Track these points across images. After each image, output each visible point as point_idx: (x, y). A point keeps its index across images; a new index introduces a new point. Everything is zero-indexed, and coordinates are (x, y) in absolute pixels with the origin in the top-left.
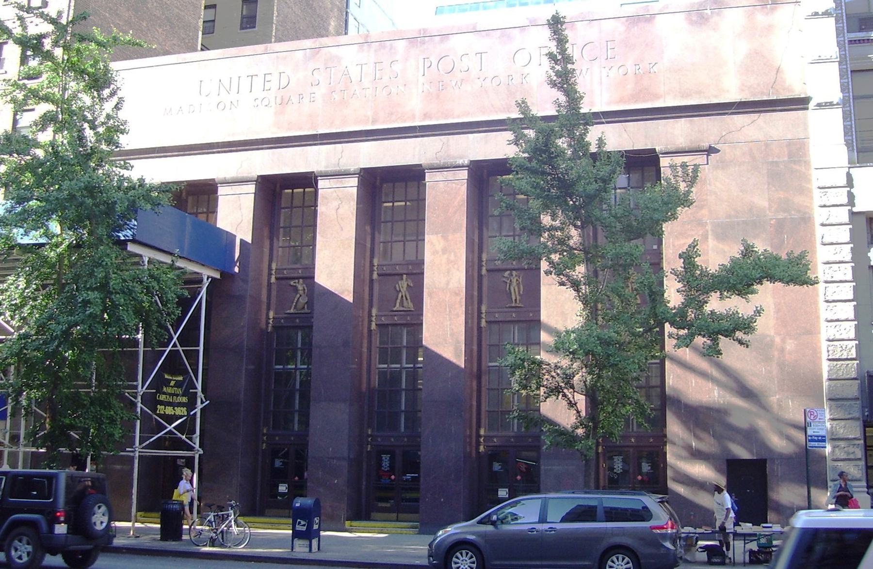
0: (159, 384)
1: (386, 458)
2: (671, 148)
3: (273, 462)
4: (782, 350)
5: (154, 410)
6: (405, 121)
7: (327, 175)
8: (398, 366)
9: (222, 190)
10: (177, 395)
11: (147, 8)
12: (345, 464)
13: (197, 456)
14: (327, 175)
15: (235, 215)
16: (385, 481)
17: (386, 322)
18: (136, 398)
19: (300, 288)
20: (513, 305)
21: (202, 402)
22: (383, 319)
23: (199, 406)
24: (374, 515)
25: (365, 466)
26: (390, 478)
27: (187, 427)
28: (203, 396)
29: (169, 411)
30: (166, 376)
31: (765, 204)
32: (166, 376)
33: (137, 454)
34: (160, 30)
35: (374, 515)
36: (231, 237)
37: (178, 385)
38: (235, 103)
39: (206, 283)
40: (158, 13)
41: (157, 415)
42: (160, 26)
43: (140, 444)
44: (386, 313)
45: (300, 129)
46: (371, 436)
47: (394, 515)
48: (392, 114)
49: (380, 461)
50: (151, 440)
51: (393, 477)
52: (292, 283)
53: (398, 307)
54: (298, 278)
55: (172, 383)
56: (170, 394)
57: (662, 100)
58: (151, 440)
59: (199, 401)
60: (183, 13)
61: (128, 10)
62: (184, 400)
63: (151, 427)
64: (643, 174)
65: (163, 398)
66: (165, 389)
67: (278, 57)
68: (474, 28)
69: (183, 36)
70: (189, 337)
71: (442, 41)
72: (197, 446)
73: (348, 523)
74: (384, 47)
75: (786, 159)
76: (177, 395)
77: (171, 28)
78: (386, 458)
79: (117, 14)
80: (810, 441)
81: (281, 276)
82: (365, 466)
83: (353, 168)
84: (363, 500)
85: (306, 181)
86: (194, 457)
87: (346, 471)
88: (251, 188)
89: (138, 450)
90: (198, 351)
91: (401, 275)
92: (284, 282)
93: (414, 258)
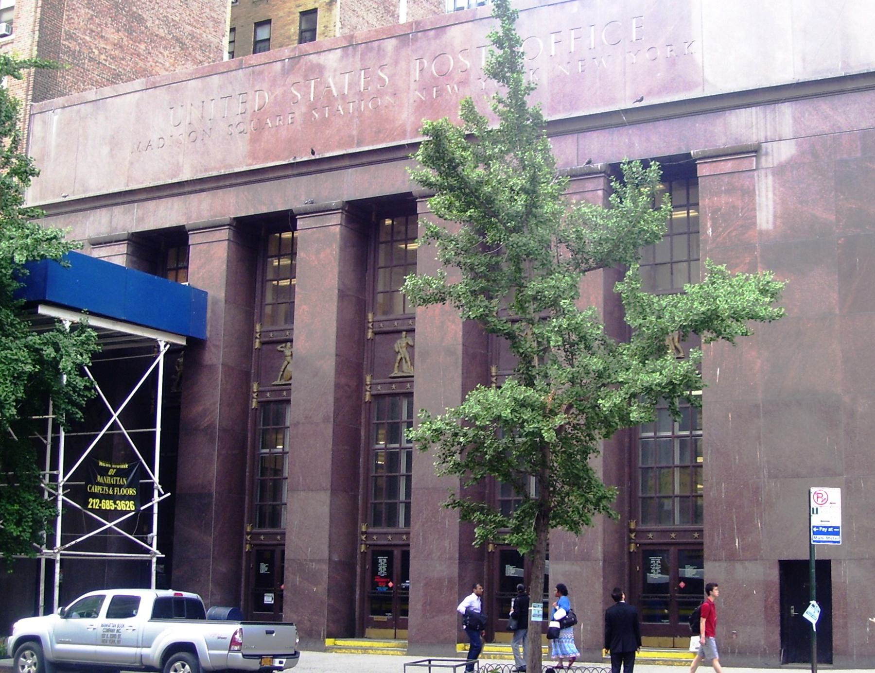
0: (89, 472)
1: (382, 561)
2: (709, 149)
3: (258, 568)
4: (852, 414)
5: (85, 504)
6: (394, 140)
7: (306, 213)
8: (397, 445)
9: (193, 239)
10: (120, 486)
11: (146, 28)
12: (325, 567)
13: (154, 560)
14: (306, 213)
15: (209, 267)
16: (382, 588)
17: (384, 392)
18: (57, 490)
21: (160, 495)
22: (379, 387)
23: (156, 499)
24: (497, 635)
25: (358, 570)
26: (387, 586)
27: (139, 523)
28: (160, 486)
29: (108, 505)
30: (101, 464)
31: (832, 218)
32: (101, 464)
33: (58, 557)
34: (166, 53)
35: (497, 635)
36: (202, 296)
37: (120, 473)
38: (208, 132)
39: (163, 350)
40: (162, 32)
41: (90, 510)
42: (165, 48)
43: (62, 544)
44: (383, 381)
45: (278, 158)
46: (365, 533)
47: (670, 640)
48: (379, 132)
49: (375, 564)
50: (79, 540)
51: (391, 584)
52: (279, 348)
53: (396, 373)
55: (112, 472)
56: (109, 486)
57: (700, 88)
58: (79, 540)
59: (156, 493)
60: (198, 31)
61: (119, 31)
62: (131, 492)
63: (76, 523)
64: (688, 194)
65: (97, 489)
66: (99, 479)
67: (253, 72)
68: (474, 16)
69: (201, 58)
70: (139, 415)
71: (437, 37)
72: (154, 548)
73: (329, 642)
74: (371, 50)
75: (859, 155)
76: (120, 486)
77: (182, 49)
78: (382, 561)
79: (102, 37)
80: (815, 533)
81: (267, 339)
82: (358, 570)
83: (334, 202)
84: (357, 614)
85: (286, 220)
86: (150, 562)
87: (326, 577)
88: (224, 234)
89: (57, 552)
90: (155, 432)
91: (400, 332)
92: (270, 347)
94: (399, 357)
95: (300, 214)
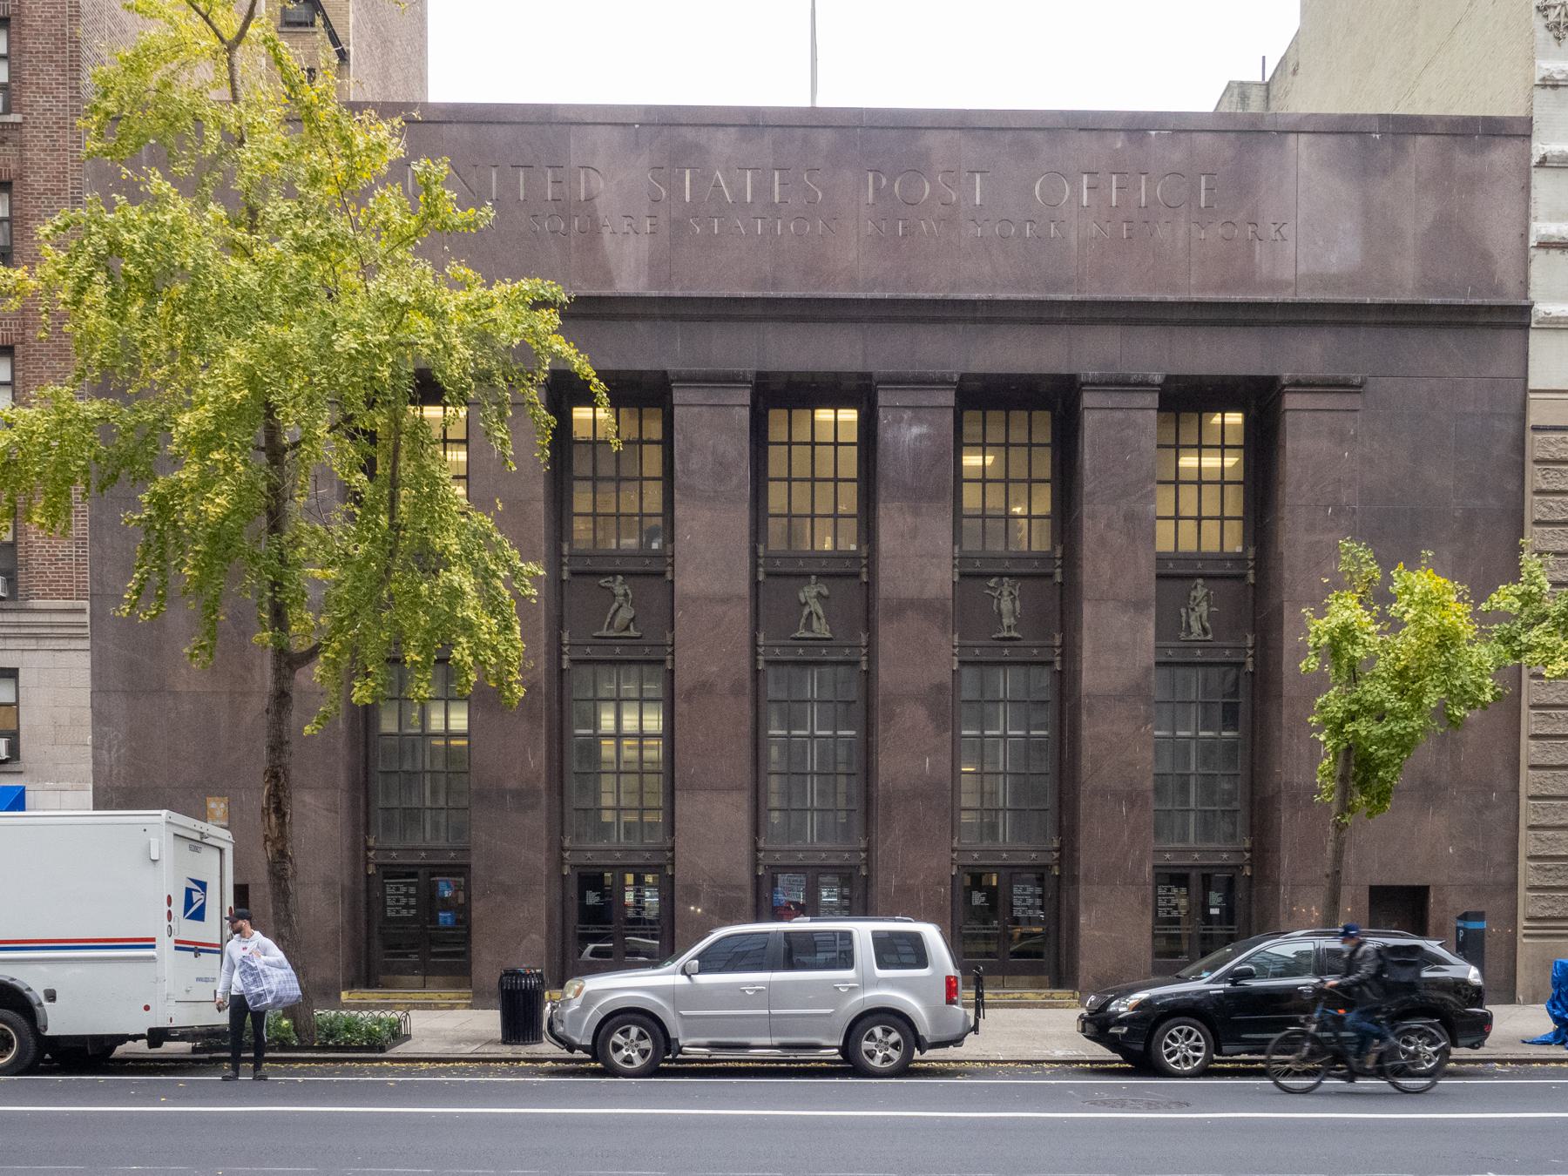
7: (692, 380)
19: (619, 590)
20: (1005, 634)
54: (614, 574)
93: (1194, 548)
94: (806, 612)
95: (680, 380)
